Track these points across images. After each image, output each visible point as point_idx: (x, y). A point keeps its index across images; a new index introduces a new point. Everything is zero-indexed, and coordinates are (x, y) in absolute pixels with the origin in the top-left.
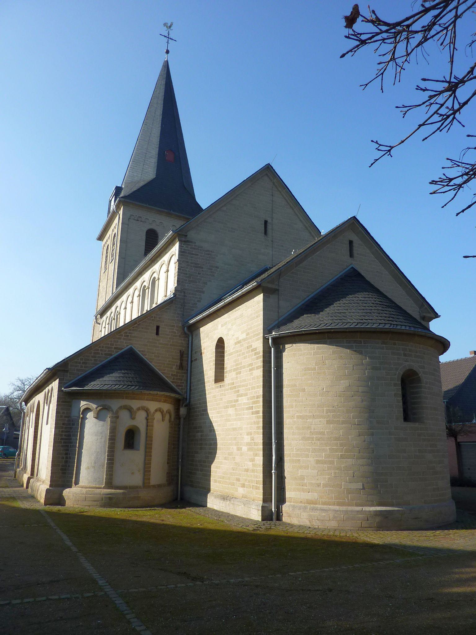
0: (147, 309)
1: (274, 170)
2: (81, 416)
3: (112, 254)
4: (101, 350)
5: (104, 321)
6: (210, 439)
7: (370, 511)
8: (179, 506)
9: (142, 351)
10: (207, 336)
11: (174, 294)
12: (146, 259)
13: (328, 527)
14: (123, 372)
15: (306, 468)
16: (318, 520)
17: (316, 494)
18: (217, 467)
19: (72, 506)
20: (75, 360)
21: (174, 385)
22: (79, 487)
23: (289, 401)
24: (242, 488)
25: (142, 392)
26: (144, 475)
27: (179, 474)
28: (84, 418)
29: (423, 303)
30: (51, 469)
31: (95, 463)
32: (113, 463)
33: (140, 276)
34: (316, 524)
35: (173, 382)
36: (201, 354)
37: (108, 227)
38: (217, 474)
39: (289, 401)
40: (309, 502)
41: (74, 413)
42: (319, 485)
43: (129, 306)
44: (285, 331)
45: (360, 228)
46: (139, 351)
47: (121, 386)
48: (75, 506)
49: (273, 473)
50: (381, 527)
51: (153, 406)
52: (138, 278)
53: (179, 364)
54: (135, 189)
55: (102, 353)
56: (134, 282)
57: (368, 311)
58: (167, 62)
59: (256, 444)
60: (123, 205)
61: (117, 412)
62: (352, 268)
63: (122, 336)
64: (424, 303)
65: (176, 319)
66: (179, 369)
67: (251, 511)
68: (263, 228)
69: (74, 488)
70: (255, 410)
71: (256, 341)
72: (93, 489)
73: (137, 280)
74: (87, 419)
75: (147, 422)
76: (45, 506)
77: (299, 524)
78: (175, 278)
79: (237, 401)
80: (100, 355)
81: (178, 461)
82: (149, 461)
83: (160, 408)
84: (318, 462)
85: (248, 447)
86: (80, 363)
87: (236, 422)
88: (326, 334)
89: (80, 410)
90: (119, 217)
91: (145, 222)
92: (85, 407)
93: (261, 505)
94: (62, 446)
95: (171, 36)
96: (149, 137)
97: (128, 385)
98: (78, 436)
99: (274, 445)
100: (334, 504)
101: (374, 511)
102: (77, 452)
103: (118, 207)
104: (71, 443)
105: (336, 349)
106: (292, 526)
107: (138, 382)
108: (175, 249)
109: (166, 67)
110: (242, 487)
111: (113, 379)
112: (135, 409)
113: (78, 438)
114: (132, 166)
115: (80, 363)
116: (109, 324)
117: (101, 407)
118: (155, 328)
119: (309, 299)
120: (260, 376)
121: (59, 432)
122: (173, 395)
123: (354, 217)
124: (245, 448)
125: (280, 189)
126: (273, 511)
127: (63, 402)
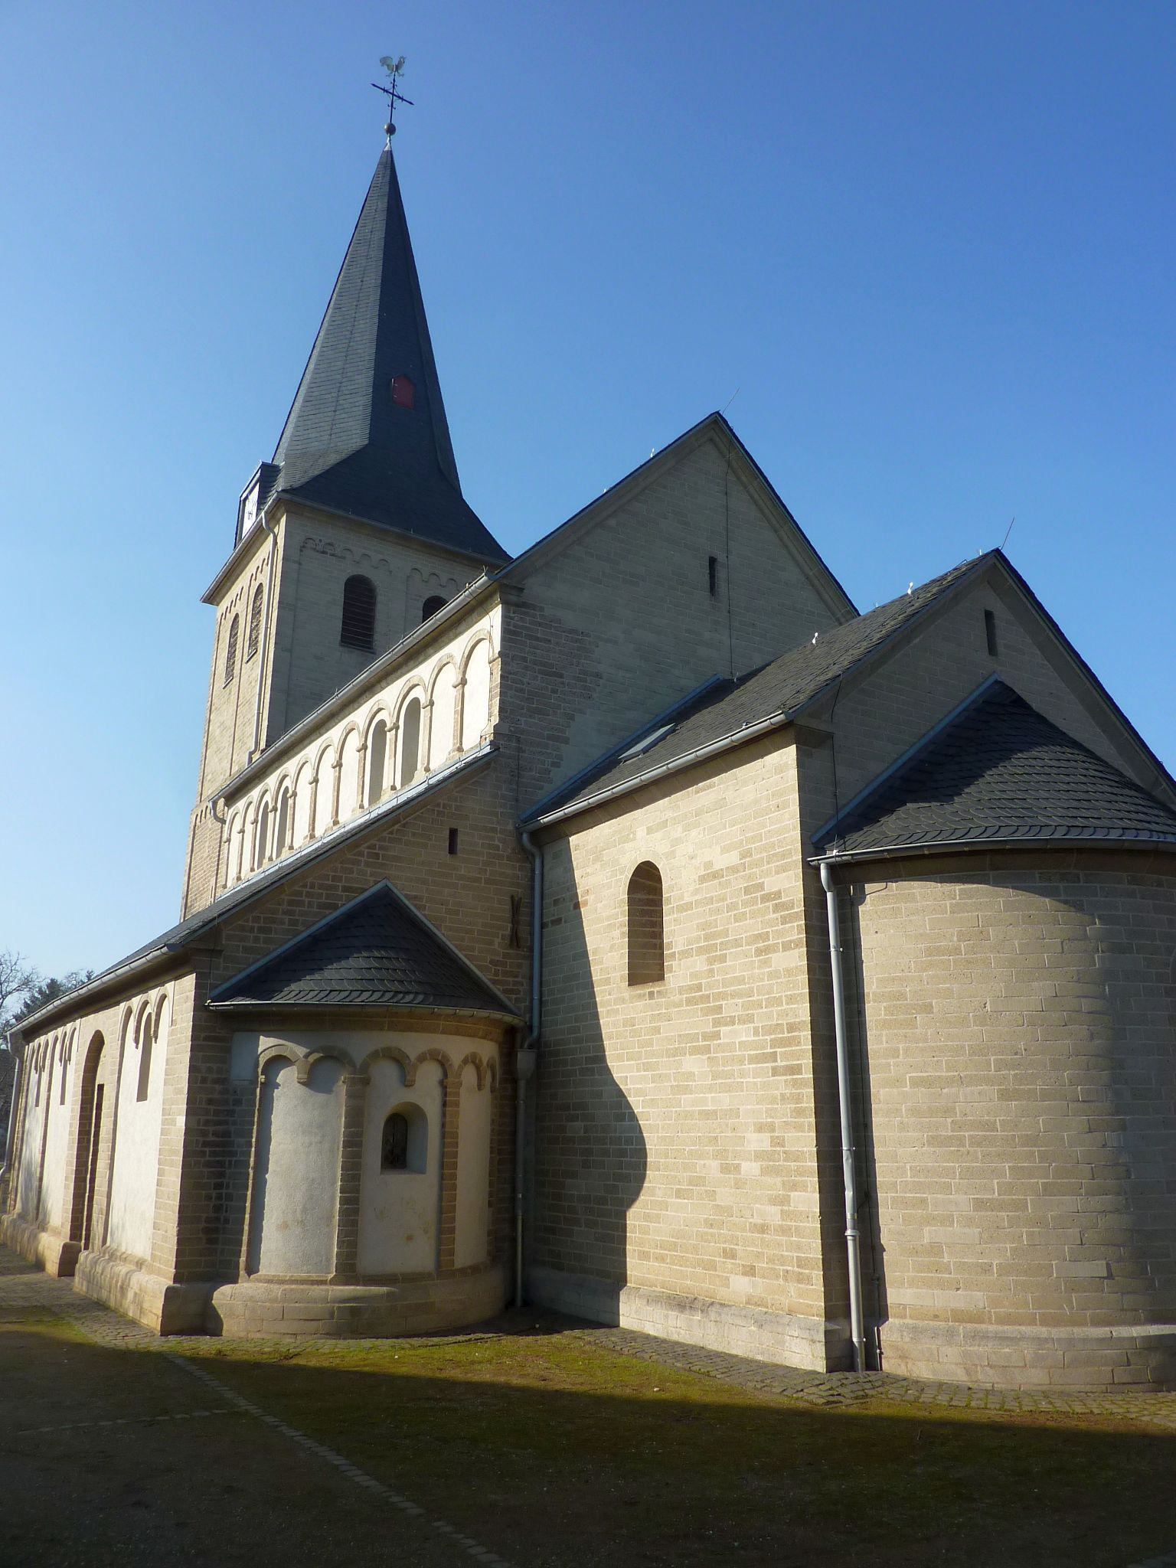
0: (392, 784)
1: (731, 430)
2: (262, 1078)
3: (250, 638)
4: (309, 895)
5: (237, 813)
6: (620, 1138)
7: (1133, 1339)
8: (537, 1326)
9: (416, 897)
10: (597, 859)
11: (492, 743)
12: (395, 651)
13: (1020, 1385)
14: (376, 954)
15: (947, 1220)
16: (990, 1367)
17: (978, 1293)
18: (647, 1217)
19: (242, 1334)
20: (240, 922)
21: (497, 990)
22: (261, 1281)
23: (884, 1039)
24: (746, 1279)
25: (436, 1010)
26: (440, 1242)
27: (516, 1233)
28: (270, 1086)
29: (1157, 779)
30: (179, 1230)
31: (304, 1210)
32: (356, 1212)
33: (367, 694)
34: (987, 1378)
35: (496, 980)
36: (577, 906)
37: (238, 565)
38: (650, 1237)
39: (884, 1039)
40: (959, 1316)
41: (239, 1070)
42: (986, 1269)
43: (327, 775)
44: (863, 845)
45: (1011, 581)
46: (406, 896)
47: (377, 995)
48: (251, 1336)
49: (849, 1238)
51: (457, 1048)
52: (361, 700)
53: (508, 932)
54: (317, 473)
55: (309, 902)
56: (346, 712)
57: (1083, 796)
58: (390, 153)
59: (798, 1157)
60: (287, 512)
61: (365, 1067)
62: (996, 682)
63: (363, 855)
64: (1161, 779)
65: (499, 810)
66: (511, 946)
67: (787, 1344)
68: (707, 578)
69: (246, 1285)
70: (784, 1063)
71: (777, 873)
72: (302, 1287)
73: (356, 705)
74: (277, 1086)
75: (445, 1094)
76: (163, 1339)
77: (935, 1377)
78: (491, 700)
79: (716, 1035)
80: (306, 909)
81: (513, 1199)
82: (450, 1202)
83: (474, 1053)
84: (980, 1205)
85: (762, 1165)
86: (252, 930)
87: (713, 1095)
88: (988, 856)
89: (258, 1061)
90: (275, 543)
91: (344, 558)
92: (273, 1053)
93: (822, 1329)
94: (208, 1164)
95: (398, 91)
96: (347, 341)
97: (397, 993)
98: (254, 1135)
99: (847, 1159)
100: (1032, 1322)
101: (1142, 1337)
102: (250, 1182)
103: (272, 518)
104: (233, 1154)
105: (1015, 896)
106: (921, 1386)
107: (420, 983)
108: (492, 621)
109: (388, 166)
110: (744, 1274)
111: (353, 975)
112: (413, 1057)
113: (254, 1140)
114: (305, 414)
115: (252, 930)
116: (257, 823)
117: (318, 1052)
118: (446, 834)
119: (905, 763)
120: (797, 968)
121: (198, 1124)
122: (497, 1015)
123: (997, 551)
124: (750, 1168)
125: (744, 479)
126: (857, 1344)
127: (206, 1039)
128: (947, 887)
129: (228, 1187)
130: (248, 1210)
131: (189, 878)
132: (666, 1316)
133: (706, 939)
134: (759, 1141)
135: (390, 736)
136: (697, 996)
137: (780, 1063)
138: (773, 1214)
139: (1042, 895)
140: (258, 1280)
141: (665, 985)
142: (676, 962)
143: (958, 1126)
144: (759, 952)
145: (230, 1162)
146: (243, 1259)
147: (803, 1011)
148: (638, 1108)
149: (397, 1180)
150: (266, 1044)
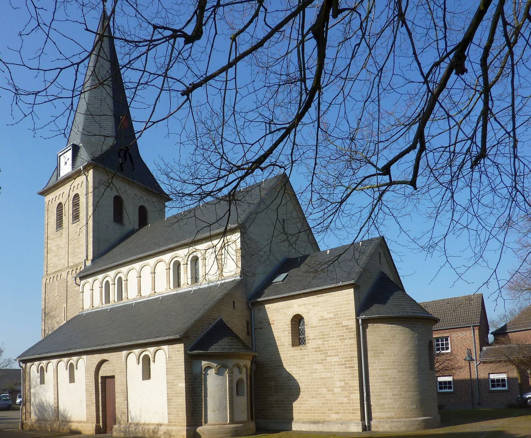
15: (386, 399)
28: (206, 374)
31: (219, 407)
33: (170, 251)
34: (395, 430)
36: (269, 324)
40: (388, 418)
42: (394, 408)
46: (225, 321)
50: (426, 428)
53: (246, 331)
61: (232, 369)
66: (247, 335)
73: (164, 253)
74: (208, 374)
84: (393, 395)
100: (403, 418)
124: (337, 390)
128: (388, 325)
129: (195, 402)
130: (203, 407)
131: (45, 303)
132: (310, 426)
133: (322, 335)
134: (339, 384)
135: (182, 267)
136: (318, 350)
137: (347, 366)
138: (345, 400)
139: (407, 328)
140: (209, 425)
141: (306, 346)
142: (311, 341)
143: (389, 379)
144: (341, 340)
145: (195, 395)
146: (203, 420)
147: (356, 354)
148: (296, 377)
149: (240, 398)
150: (204, 363)
